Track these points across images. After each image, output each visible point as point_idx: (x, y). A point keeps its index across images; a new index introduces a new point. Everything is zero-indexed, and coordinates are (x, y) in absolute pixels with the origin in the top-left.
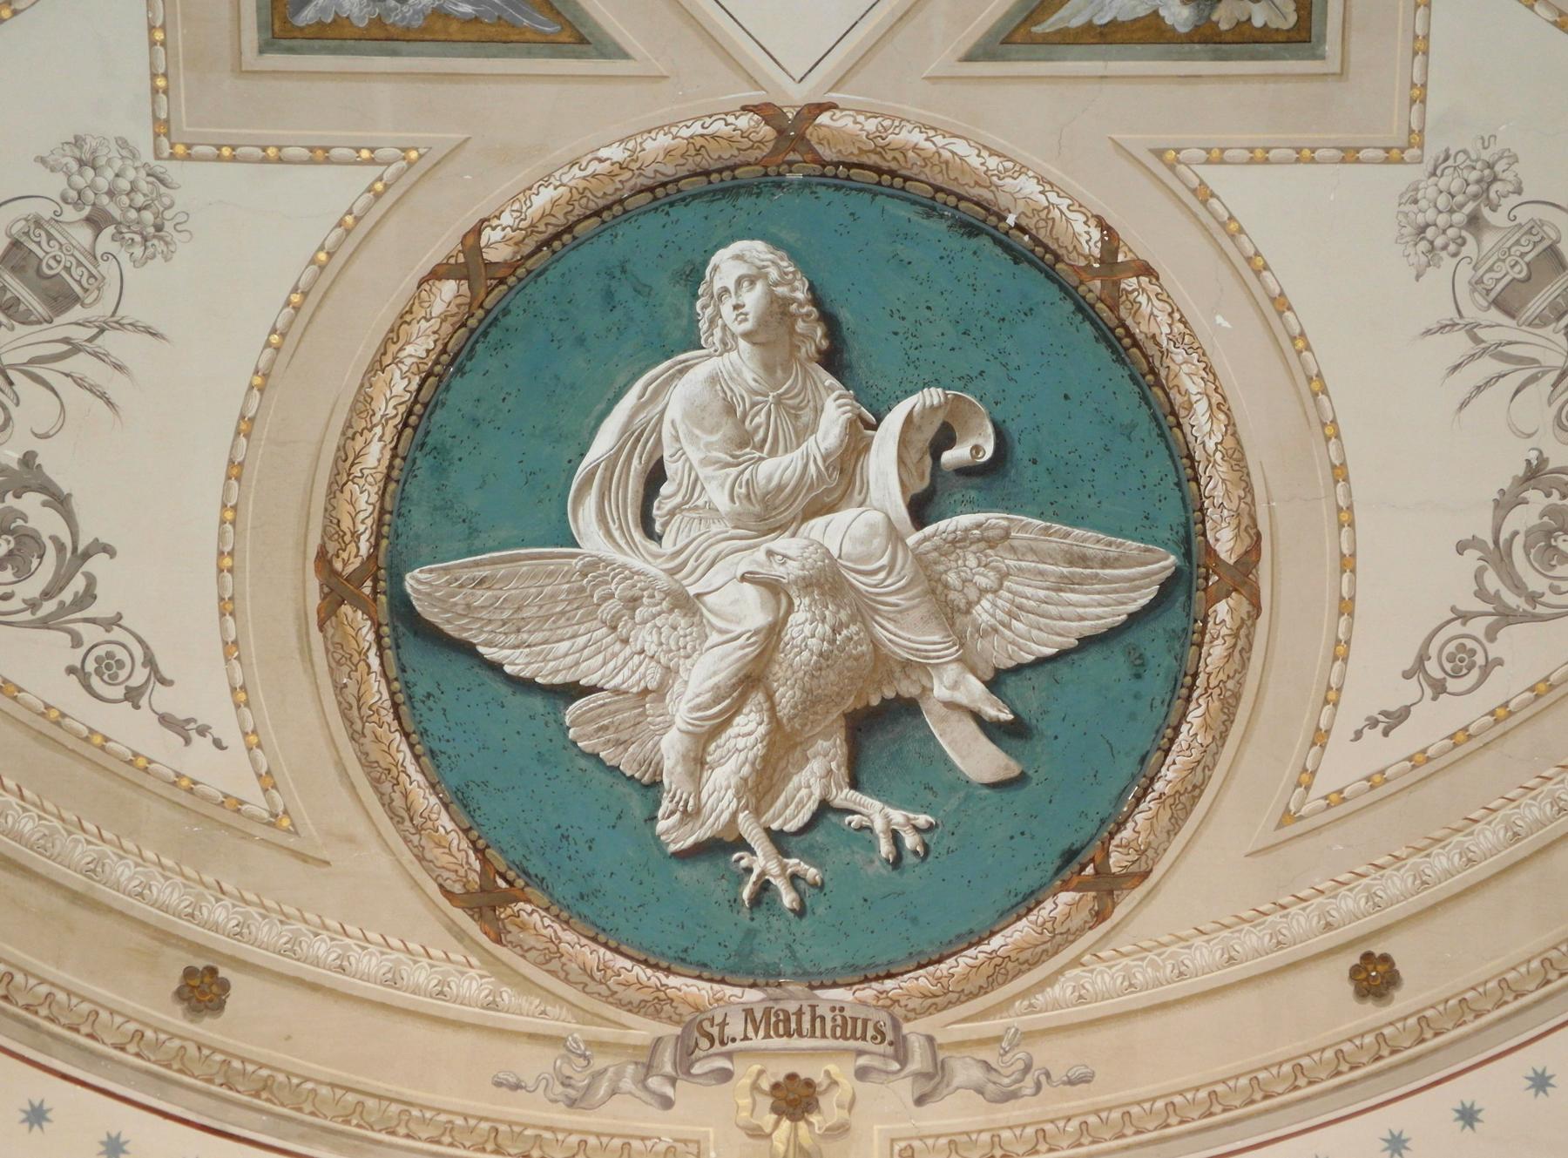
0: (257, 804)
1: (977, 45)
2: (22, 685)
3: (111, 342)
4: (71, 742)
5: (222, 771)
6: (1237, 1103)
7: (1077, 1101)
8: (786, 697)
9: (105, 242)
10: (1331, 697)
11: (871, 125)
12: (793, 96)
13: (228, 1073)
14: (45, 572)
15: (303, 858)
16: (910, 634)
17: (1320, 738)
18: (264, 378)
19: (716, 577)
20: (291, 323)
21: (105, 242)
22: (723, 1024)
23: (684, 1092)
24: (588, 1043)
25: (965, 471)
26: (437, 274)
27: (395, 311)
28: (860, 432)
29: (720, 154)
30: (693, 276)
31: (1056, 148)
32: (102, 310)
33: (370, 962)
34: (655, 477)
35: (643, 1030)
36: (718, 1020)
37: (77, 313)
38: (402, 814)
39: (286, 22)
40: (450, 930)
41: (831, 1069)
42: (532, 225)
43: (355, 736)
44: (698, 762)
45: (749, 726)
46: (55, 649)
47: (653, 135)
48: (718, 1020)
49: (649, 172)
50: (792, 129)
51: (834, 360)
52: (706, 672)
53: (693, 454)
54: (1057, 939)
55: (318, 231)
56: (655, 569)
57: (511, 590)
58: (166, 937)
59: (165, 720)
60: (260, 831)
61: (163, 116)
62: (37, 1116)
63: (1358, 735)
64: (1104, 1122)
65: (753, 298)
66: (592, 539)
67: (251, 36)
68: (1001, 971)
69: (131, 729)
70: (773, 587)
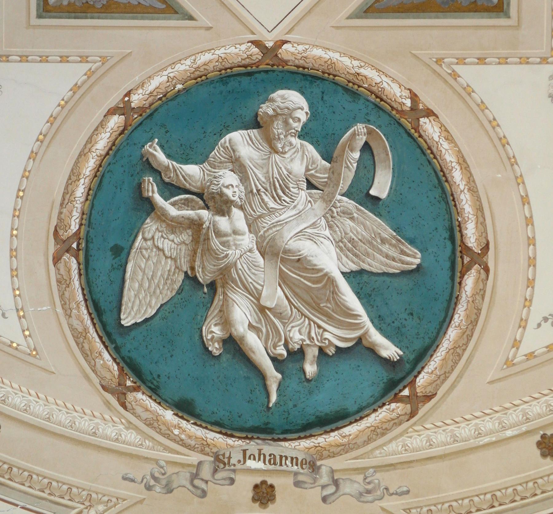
1: (350, 15)
2: (74, 83)
6: (485, 507)
10: (528, 302)
11: (301, 48)
17: (523, 324)
20: (58, 114)
22: (229, 458)
24: (167, 462)
31: (390, 59)
35: (194, 458)
36: (227, 455)
39: (45, 9)
40: (105, 403)
42: (151, 93)
47: (204, 53)
48: (227, 455)
49: (202, 69)
61: (539, 60)
63: (539, 325)
64: (505, 495)
67: (502, 22)
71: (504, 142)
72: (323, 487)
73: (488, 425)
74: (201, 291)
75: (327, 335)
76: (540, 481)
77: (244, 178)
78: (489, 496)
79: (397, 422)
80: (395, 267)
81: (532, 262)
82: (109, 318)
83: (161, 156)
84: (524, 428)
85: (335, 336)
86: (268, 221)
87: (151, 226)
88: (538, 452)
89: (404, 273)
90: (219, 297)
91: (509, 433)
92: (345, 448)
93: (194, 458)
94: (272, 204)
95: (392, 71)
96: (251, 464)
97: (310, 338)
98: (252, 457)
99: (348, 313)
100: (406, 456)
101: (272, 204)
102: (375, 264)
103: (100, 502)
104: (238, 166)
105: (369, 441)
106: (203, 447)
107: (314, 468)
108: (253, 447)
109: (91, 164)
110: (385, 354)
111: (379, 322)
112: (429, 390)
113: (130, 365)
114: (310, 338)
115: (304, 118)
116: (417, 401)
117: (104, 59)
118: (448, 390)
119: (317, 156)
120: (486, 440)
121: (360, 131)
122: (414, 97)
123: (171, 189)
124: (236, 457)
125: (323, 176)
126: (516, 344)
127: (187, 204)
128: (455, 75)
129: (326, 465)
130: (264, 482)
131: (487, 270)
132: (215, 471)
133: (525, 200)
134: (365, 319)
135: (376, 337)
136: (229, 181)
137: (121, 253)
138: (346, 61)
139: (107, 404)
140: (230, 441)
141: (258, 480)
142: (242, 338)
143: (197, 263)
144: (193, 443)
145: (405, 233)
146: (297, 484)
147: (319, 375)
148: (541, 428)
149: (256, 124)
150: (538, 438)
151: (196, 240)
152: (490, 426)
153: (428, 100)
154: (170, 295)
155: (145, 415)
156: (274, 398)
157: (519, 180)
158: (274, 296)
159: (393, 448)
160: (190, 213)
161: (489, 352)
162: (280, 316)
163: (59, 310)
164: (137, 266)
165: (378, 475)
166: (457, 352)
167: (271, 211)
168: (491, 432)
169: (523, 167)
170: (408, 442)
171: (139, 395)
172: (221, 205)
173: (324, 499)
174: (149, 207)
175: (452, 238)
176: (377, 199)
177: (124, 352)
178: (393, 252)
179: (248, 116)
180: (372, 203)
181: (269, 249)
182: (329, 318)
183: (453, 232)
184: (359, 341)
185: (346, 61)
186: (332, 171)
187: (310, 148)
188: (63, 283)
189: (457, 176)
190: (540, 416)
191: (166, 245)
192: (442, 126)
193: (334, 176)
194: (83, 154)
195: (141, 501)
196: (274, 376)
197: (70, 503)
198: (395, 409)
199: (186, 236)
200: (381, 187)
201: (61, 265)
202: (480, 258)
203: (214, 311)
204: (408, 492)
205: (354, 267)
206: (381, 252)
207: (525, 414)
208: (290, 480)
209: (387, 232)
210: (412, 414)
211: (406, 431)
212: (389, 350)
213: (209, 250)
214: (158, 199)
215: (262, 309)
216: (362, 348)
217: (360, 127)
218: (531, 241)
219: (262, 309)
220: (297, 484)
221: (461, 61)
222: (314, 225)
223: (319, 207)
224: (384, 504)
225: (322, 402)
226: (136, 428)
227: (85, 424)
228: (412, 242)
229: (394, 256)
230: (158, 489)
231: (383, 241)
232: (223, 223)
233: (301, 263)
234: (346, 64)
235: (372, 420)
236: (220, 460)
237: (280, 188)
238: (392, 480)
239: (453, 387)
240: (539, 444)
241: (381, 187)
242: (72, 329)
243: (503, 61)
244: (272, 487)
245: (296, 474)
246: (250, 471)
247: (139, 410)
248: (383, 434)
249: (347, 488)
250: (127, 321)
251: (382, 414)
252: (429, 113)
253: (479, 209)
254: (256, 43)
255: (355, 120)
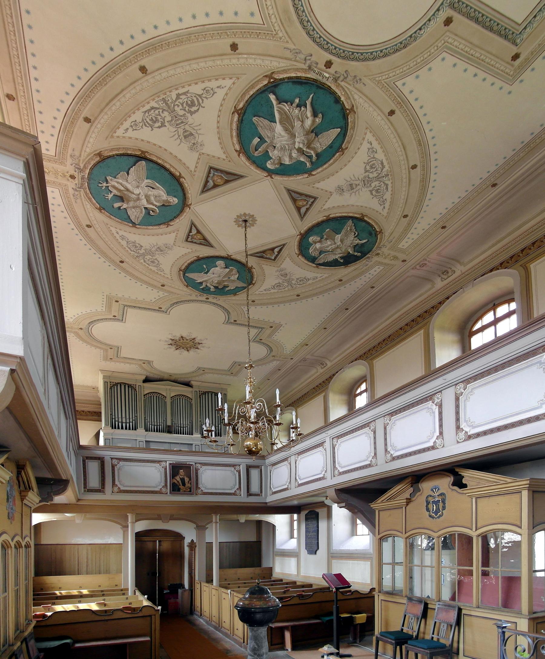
0: (114, 135)
3: (179, 141)
4: (126, 117)
5: (120, 132)
7: (74, 203)
8: (126, 192)
9: (191, 144)
10: (226, 94)
12: (192, 207)
13: (73, 122)
14: (150, 122)
15: (107, 137)
16: (131, 204)
17: (230, 89)
18: (171, 154)
19: (141, 191)
21: (191, 144)
23: (73, 167)
25: (149, 212)
26: (180, 174)
27: (177, 169)
28: (156, 206)
29: (187, 200)
30: (175, 197)
32: (183, 140)
33: (91, 140)
34: (153, 188)
35: (343, 84)
37: (183, 138)
38: (112, 150)
41: (76, 181)
43: (123, 148)
44: (118, 183)
45: (122, 188)
46: (139, 119)
50: (189, 206)
51: (163, 205)
52: (129, 186)
53: (155, 192)
54: (94, 204)
55: (188, 164)
56: (142, 185)
57: (141, 171)
58: (96, 118)
59: (128, 129)
60: (111, 134)
62: (236, 14)
65: (171, 201)
66: (146, 181)
67: (211, 165)
68: (89, 199)
69: (127, 124)
70: (139, 195)
71: (219, 138)
72: (310, 60)
73: (251, 61)
74: (316, 131)
75: (288, 108)
76: (241, 36)
77: (290, 154)
78: (259, 37)
79: (279, 72)
80: (261, 119)
81: (221, 105)
82: (343, 132)
83: (308, 164)
84: (240, 56)
85: (286, 107)
86: (289, 143)
87: (319, 150)
88: (238, 46)
89: (260, 117)
90: (312, 129)
91: (245, 56)
92: (297, 70)
93: (343, 84)
94: (287, 146)
95: (242, 163)
96: (327, 75)
97: (293, 109)
98: (326, 77)
99: (279, 112)
100: (280, 60)
101: (287, 146)
102: (266, 122)
103: (376, 81)
104: (290, 157)
105: (289, 70)
106: (338, 86)
107: (310, 67)
108: (324, 81)
109: (325, 166)
110: (274, 97)
111: (272, 106)
112: (265, 78)
113: (345, 117)
114: (293, 109)
115: (269, 162)
116: (270, 76)
117: (309, 186)
118: (370, 370)
119: (270, 153)
120: (253, 56)
121: (256, 154)
122: (239, 156)
123: (310, 157)
124: (330, 79)
125: (271, 148)
126: (234, 83)
127: (308, 153)
128: (227, 157)
129: (305, 67)
130: (327, 68)
131: (235, 107)
132: (339, 77)
133: (218, 122)
134: (275, 109)
135: (274, 102)
136: (295, 154)
137: (331, 146)
138: (252, 168)
139: (357, 108)
140: (330, 85)
141: (328, 70)
142: (311, 116)
143: (313, 139)
144: (341, 88)
145: (255, 127)
146: (317, 64)
147: (295, 98)
148: (234, 54)
149: (281, 164)
150: (237, 51)
151: (310, 144)
152: (251, 61)
153: (236, 154)
154: (324, 133)
155: (349, 101)
156: (311, 96)
157: (218, 128)
158: (297, 124)
159: (283, 64)
160: (308, 150)
161: (243, 83)
162: (299, 119)
163: (354, 136)
164: (328, 142)
165: (291, 57)
166: (252, 87)
167: (288, 145)
168: (251, 58)
169: (216, 130)
170: (278, 65)
171: (347, 107)
172: (300, 150)
173: (311, 55)
174: (318, 155)
175: (242, 120)
176: (259, 138)
177: (344, 122)
178: (260, 123)
179: (282, 167)
180: (260, 137)
181: (293, 136)
182: (285, 113)
183: (241, 121)
184: (279, 103)
185: (252, 168)
186: (268, 148)
187: (270, 155)
188: (349, 142)
189: (234, 134)
190: (234, 58)
191: (318, 145)
192: (234, 147)
193: (267, 147)
194: (326, 169)
195: (365, 76)
196: (308, 103)
197: (385, 85)
198: (276, 76)
199: (312, 145)
200: (256, 140)
201: (347, 146)
202: (236, 111)
203: (315, 126)
204: (285, 48)
205: (272, 123)
206: (264, 124)
207: (238, 61)
208: (319, 66)
209: (259, 129)
210: (273, 73)
211: (277, 68)
212: (272, 97)
213: (308, 141)
214: (314, 156)
215: (302, 122)
216: (280, 101)
217: (256, 155)
218: (220, 111)
219: (302, 122)
220: (317, 64)
221: (224, 160)
222: (278, 138)
223: (275, 141)
224: (294, 47)
225: (299, 89)
226: (353, 98)
227: (366, 105)
228: (254, 124)
229: (261, 123)
230: (358, 78)
231: (262, 127)
232: (301, 146)
233: (286, 130)
234: (253, 168)
235: (285, 76)
236: (336, 80)
237: (283, 149)
238: (288, 54)
239: (258, 76)
240: (237, 49)
241: (256, 140)
242: (354, 131)
243: (214, 157)
244: (325, 66)
245: (316, 67)
246: (329, 73)
247: (350, 103)
248: (284, 70)
249: (303, 57)
250: (339, 130)
251: (281, 76)
252: (236, 151)
253: (231, 124)
254: (272, 178)
255: (257, 157)
